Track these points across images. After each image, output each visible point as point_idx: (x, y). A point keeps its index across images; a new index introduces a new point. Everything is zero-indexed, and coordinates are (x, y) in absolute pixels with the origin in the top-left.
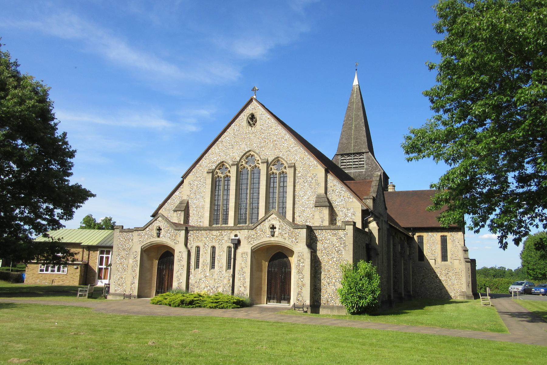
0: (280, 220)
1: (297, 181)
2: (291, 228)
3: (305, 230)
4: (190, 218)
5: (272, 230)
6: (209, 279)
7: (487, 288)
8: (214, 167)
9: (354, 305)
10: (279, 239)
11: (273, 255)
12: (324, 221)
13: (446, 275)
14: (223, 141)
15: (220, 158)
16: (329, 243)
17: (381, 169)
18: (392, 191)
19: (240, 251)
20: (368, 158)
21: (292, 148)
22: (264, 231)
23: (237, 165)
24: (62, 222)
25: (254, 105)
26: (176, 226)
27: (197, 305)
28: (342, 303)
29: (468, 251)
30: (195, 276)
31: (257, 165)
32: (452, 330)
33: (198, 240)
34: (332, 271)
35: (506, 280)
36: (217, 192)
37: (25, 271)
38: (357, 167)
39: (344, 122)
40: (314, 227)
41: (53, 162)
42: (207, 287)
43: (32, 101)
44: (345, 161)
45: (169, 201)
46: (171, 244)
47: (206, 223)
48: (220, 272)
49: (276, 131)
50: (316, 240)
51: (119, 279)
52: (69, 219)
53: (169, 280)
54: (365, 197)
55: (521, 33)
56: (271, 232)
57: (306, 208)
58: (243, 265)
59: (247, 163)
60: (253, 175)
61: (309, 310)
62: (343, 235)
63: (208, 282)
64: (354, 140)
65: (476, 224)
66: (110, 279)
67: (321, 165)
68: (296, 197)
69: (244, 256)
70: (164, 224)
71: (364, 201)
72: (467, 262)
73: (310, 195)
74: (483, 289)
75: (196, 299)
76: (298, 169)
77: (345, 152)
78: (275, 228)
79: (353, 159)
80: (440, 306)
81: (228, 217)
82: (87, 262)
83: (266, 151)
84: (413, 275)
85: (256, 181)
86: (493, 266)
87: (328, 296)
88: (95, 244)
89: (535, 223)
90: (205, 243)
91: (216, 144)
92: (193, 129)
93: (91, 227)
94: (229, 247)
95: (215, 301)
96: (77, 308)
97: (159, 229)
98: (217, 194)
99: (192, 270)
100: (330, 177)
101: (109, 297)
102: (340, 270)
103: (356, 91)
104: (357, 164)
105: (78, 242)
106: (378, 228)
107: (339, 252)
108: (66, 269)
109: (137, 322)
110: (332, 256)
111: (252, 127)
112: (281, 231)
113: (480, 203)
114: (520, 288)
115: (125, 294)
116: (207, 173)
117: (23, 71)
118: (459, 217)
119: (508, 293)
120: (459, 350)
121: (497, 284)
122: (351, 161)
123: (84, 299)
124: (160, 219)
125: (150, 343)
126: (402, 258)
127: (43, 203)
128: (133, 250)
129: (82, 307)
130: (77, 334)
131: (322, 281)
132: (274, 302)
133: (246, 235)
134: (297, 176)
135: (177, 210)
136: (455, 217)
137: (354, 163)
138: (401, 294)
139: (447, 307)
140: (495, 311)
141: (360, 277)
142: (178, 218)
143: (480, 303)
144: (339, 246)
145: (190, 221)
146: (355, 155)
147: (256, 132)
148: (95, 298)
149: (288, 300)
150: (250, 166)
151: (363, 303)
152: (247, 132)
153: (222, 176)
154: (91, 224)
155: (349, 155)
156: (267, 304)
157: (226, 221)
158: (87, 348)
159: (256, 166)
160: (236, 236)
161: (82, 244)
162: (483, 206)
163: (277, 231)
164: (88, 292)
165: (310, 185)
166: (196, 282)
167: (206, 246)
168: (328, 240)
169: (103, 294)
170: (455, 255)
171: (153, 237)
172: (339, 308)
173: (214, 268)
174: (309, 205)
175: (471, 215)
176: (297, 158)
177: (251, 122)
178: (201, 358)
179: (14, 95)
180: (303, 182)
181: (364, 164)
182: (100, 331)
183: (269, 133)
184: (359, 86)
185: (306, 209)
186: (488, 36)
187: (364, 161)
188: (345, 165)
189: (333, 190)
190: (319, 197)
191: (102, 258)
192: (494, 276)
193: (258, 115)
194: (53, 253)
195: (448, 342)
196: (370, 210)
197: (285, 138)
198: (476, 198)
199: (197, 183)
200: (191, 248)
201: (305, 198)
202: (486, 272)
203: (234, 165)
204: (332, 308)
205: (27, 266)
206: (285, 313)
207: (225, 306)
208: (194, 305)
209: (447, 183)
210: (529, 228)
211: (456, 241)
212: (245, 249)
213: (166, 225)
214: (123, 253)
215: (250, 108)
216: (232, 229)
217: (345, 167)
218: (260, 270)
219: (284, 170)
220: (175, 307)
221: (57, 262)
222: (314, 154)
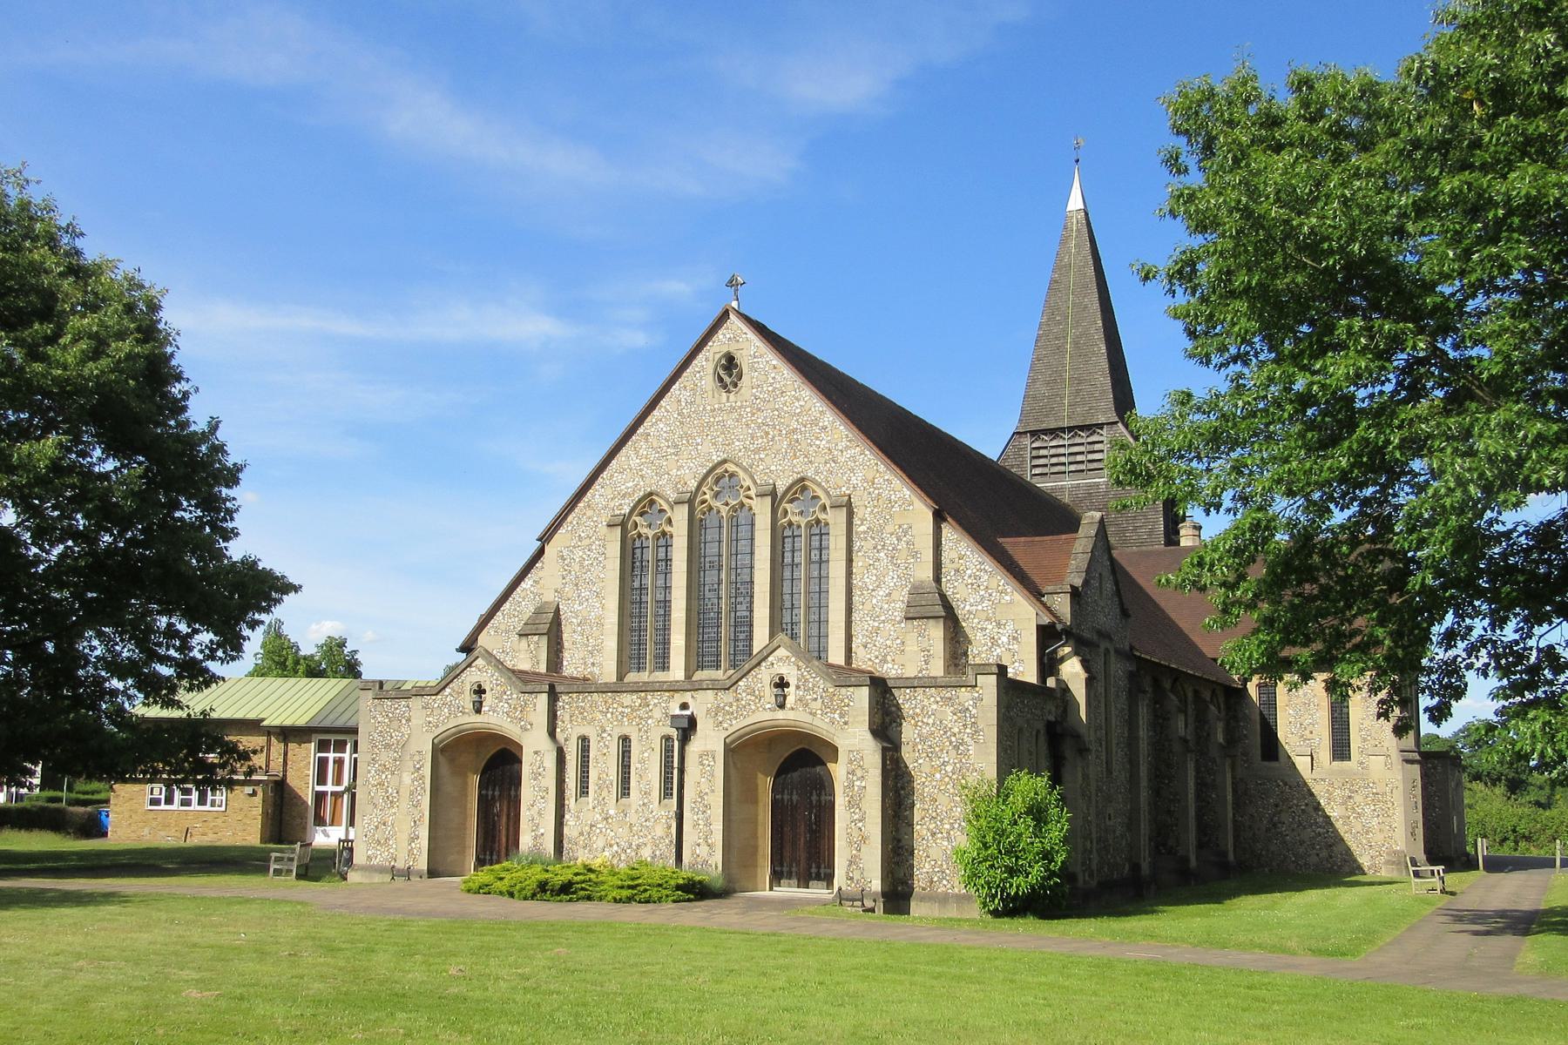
0: (800, 664)
1: (857, 545)
3: (865, 691)
4: (566, 655)
5: (779, 691)
8: (626, 510)
9: (996, 892)
10: (796, 715)
15: (642, 483)
16: (933, 724)
18: (1190, 544)
19: (694, 748)
21: (842, 451)
22: (757, 692)
23: (691, 502)
24: (213, 666)
26: (524, 679)
27: (582, 893)
31: (746, 501)
33: (584, 718)
34: (943, 800)
37: (107, 801)
38: (1083, 471)
39: (1040, 329)
40: (892, 681)
41: (185, 503)
42: (611, 846)
44: (1043, 452)
45: (507, 606)
46: (510, 729)
47: (607, 670)
48: (644, 804)
49: (796, 404)
50: (898, 716)
52: (233, 659)
53: (511, 829)
54: (1050, 588)
57: (883, 622)
58: (705, 788)
59: (716, 495)
60: (734, 529)
61: (880, 906)
63: (613, 834)
66: (352, 823)
68: (856, 592)
70: (492, 676)
73: (892, 584)
76: (859, 513)
77: (1044, 426)
78: (787, 685)
81: (669, 649)
82: (281, 775)
83: (768, 460)
85: (743, 546)
88: (302, 721)
91: (630, 443)
94: (668, 738)
95: (631, 883)
96: (277, 902)
97: (480, 691)
99: (570, 801)
101: (353, 877)
103: (1078, 230)
104: (1082, 462)
105: (251, 716)
106: (1086, 675)
109: (427, 932)
111: (729, 392)
112: (801, 693)
115: (393, 867)
116: (609, 526)
117: (92, 251)
121: (1554, 827)
122: (1061, 451)
123: (286, 881)
124: (480, 662)
125: (452, 971)
127: (160, 613)
128: (413, 748)
129: (291, 902)
130: (295, 955)
131: (917, 828)
132: (790, 886)
133: (709, 706)
134: (857, 532)
137: (1072, 459)
141: (1013, 815)
142: (530, 656)
144: (959, 733)
145: (565, 663)
146: (1076, 433)
147: (740, 408)
148: (317, 879)
149: (829, 879)
150: (727, 504)
152: (716, 406)
153: (650, 533)
154: (286, 660)
155: (1054, 432)
156: (771, 889)
157: (663, 663)
158: (323, 978)
159: (742, 505)
160: (684, 706)
161: (265, 723)
164: (295, 863)
165: (893, 558)
166: (581, 834)
167: (604, 735)
168: (929, 717)
170: (1373, 742)
171: (463, 713)
172: (961, 899)
173: (629, 794)
174: (890, 613)
176: (855, 482)
177: (727, 379)
178: (555, 996)
179: (80, 332)
180: (875, 548)
182: (343, 950)
184: (1086, 214)
185: (882, 625)
187: (1102, 451)
188: (1046, 465)
189: (957, 571)
190: (916, 591)
191: (322, 763)
193: (746, 358)
194: (193, 751)
196: (1059, 627)
197: (821, 424)
199: (581, 553)
200: (566, 740)
201: (881, 593)
204: (944, 899)
205: (113, 791)
207: (655, 895)
208: (574, 893)
212: (709, 743)
213: (497, 680)
214: (385, 757)
215: (721, 337)
216: (673, 688)
217: (1045, 470)
218: (751, 797)
219: (822, 516)
220: (525, 899)
221: (208, 780)
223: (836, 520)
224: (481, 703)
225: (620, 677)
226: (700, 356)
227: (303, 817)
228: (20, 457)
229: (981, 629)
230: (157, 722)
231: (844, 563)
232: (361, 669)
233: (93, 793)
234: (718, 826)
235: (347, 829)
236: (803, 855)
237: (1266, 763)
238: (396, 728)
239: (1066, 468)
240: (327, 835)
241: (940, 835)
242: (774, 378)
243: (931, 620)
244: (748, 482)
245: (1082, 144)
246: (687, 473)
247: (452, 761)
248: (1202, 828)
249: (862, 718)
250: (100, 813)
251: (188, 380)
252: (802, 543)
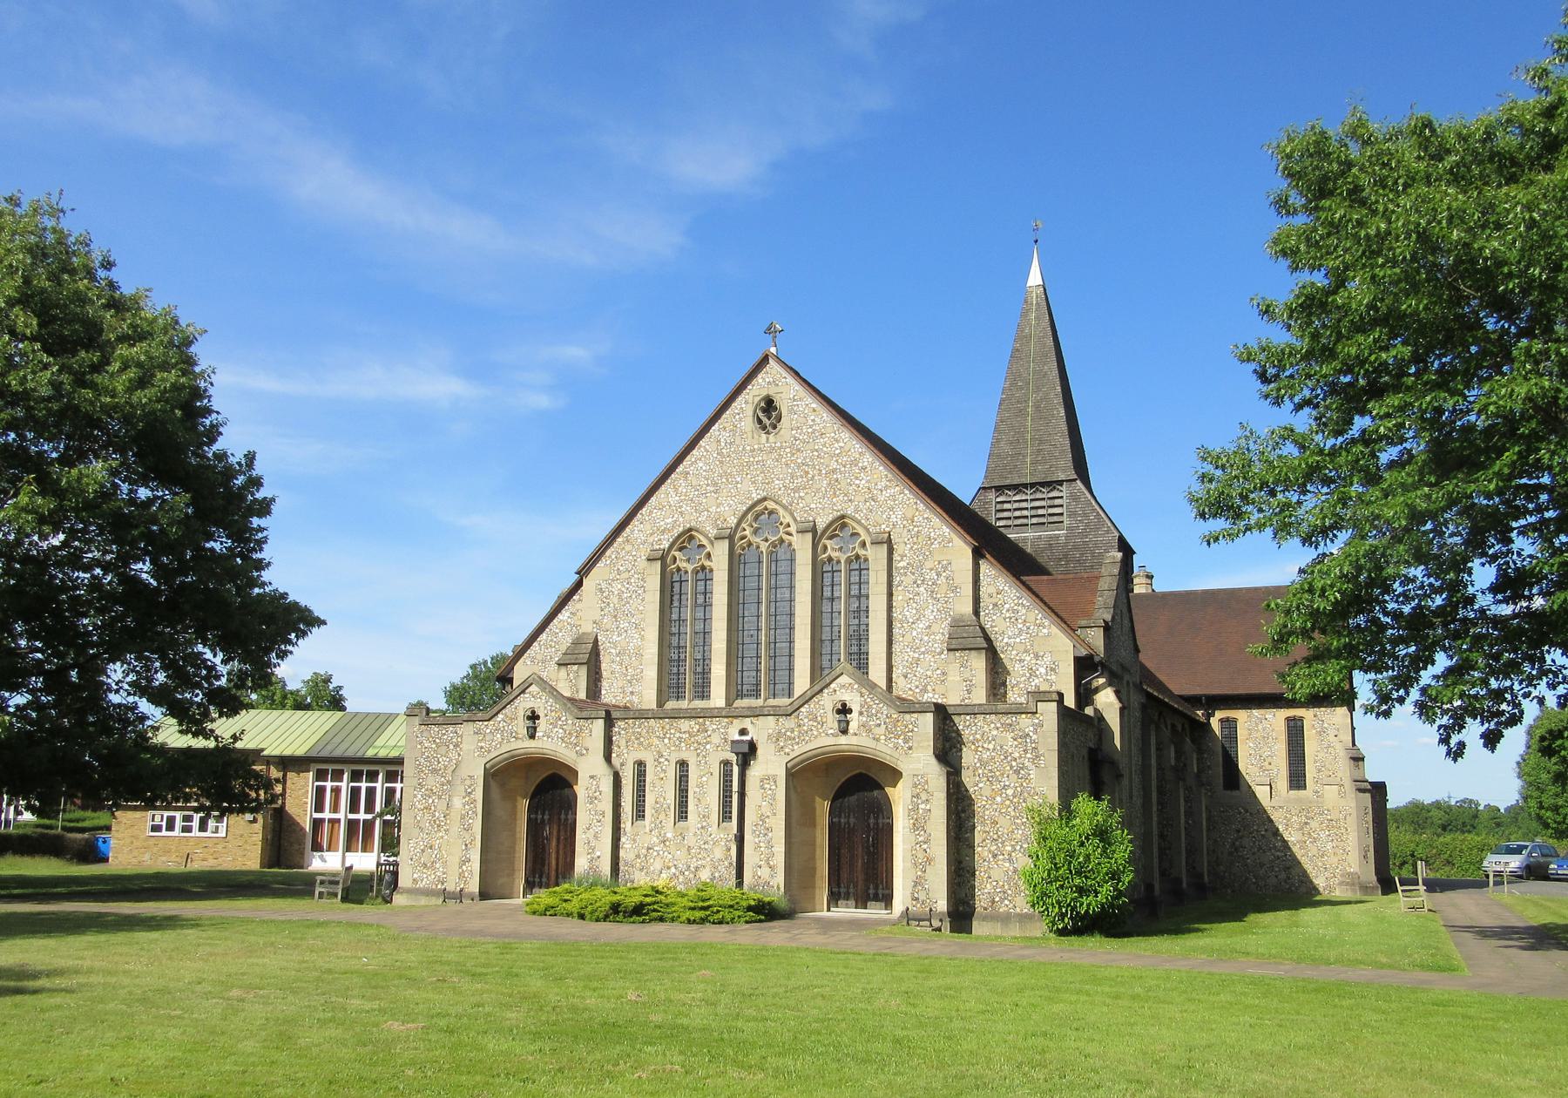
0: (863, 690)
2: (893, 711)
3: (930, 717)
4: (605, 684)
5: (842, 717)
6: (673, 850)
7: (1419, 862)
8: (666, 545)
9: (1067, 911)
10: (860, 740)
11: (843, 783)
12: (973, 689)
13: (1301, 829)
14: (688, 473)
15: (681, 519)
17: (1112, 528)
19: (755, 771)
20: (1074, 497)
22: (819, 718)
23: (731, 538)
25: (774, 372)
27: (655, 914)
28: (1033, 906)
29: (1363, 759)
30: (634, 840)
31: (785, 537)
32: (1323, 967)
33: (641, 744)
34: (1004, 822)
35: (1473, 838)
36: (675, 610)
37: (108, 828)
40: (952, 708)
42: (669, 868)
43: (170, 372)
44: (1006, 506)
45: (543, 636)
46: (565, 754)
47: (647, 697)
48: (702, 827)
49: (836, 445)
51: (423, 851)
54: (1083, 623)
55: (1487, 251)
56: (839, 721)
57: (923, 653)
58: (766, 810)
59: (756, 532)
61: (947, 925)
62: (1031, 729)
64: (1032, 446)
65: (1384, 698)
67: (959, 537)
68: (896, 625)
69: (768, 786)
71: (1079, 632)
72: (1361, 790)
73: (932, 617)
74: (1408, 867)
75: (648, 900)
76: (899, 549)
77: (1008, 482)
78: (850, 711)
79: (1032, 500)
80: (1288, 912)
83: (808, 499)
84: (1208, 830)
85: (783, 579)
86: (1439, 798)
87: (995, 888)
88: (301, 752)
89: (1535, 693)
90: (659, 752)
92: (543, 401)
93: (274, 701)
94: (726, 764)
95: (701, 904)
97: (533, 717)
98: (675, 616)
99: (626, 824)
100: (988, 569)
101: (399, 899)
102: (1025, 820)
106: (1120, 705)
107: (1022, 772)
108: (223, 826)
110: (1002, 784)
111: (768, 433)
112: (864, 719)
113: (1396, 641)
114: (1515, 862)
118: (1342, 680)
119: (1479, 876)
120: (1342, 1007)
122: (1024, 505)
123: (332, 903)
126: (1181, 783)
128: (464, 772)
131: (978, 849)
133: (770, 731)
134: (896, 568)
136: (1329, 679)
137: (1034, 512)
138: (1178, 881)
139: (1307, 915)
140: (1437, 924)
141: (1080, 837)
142: (573, 683)
143: (1397, 905)
144: (1020, 757)
145: (603, 692)
147: (780, 448)
149: (887, 900)
150: (766, 540)
151: (1089, 905)
152: (756, 447)
153: (690, 568)
154: (274, 694)
155: (1017, 488)
156: (829, 910)
157: (703, 691)
159: (782, 541)
160: (743, 732)
161: (265, 753)
162: (1402, 651)
163: (854, 720)
164: (341, 886)
166: (638, 856)
167: (662, 760)
168: (990, 742)
169: (372, 891)
171: (517, 738)
172: (1023, 918)
173: (686, 817)
175: (1372, 676)
177: (765, 420)
180: (915, 583)
181: (1062, 514)
183: (817, 451)
184: (1045, 290)
186: (1408, 257)
187: (1062, 506)
189: (995, 605)
190: (957, 624)
191: (320, 792)
192: (1444, 828)
195: (1316, 991)
196: (1097, 659)
197: (860, 465)
198: (1383, 628)
199: (619, 586)
200: (622, 765)
201: (921, 626)
202: (1418, 815)
203: (723, 538)
204: (1006, 919)
205: (115, 818)
206: (889, 933)
208: (646, 914)
209: (1307, 600)
210: (1520, 704)
211: (1332, 733)
212: (770, 768)
213: (551, 706)
214: (432, 781)
215: (760, 381)
216: (729, 713)
217: (1009, 523)
218: (810, 820)
219: (862, 552)
222: (941, 508)
223: (876, 556)
224: (535, 728)
225: (660, 704)
226: (740, 398)
227: (301, 843)
228: (68, 482)
229: (1020, 661)
230: (188, 752)
231: (885, 597)
232: (346, 704)
233: (78, 821)
234: (780, 849)
235: (344, 855)
236: (860, 876)
237: (1229, 792)
239: (1029, 521)
240: (324, 860)
241: (1001, 857)
243: (973, 652)
244: (788, 519)
245: (1040, 226)
246: (728, 510)
247: (502, 785)
248: (1189, 852)
249: (927, 743)
250: (97, 839)
251: (218, 413)
252: (842, 577)
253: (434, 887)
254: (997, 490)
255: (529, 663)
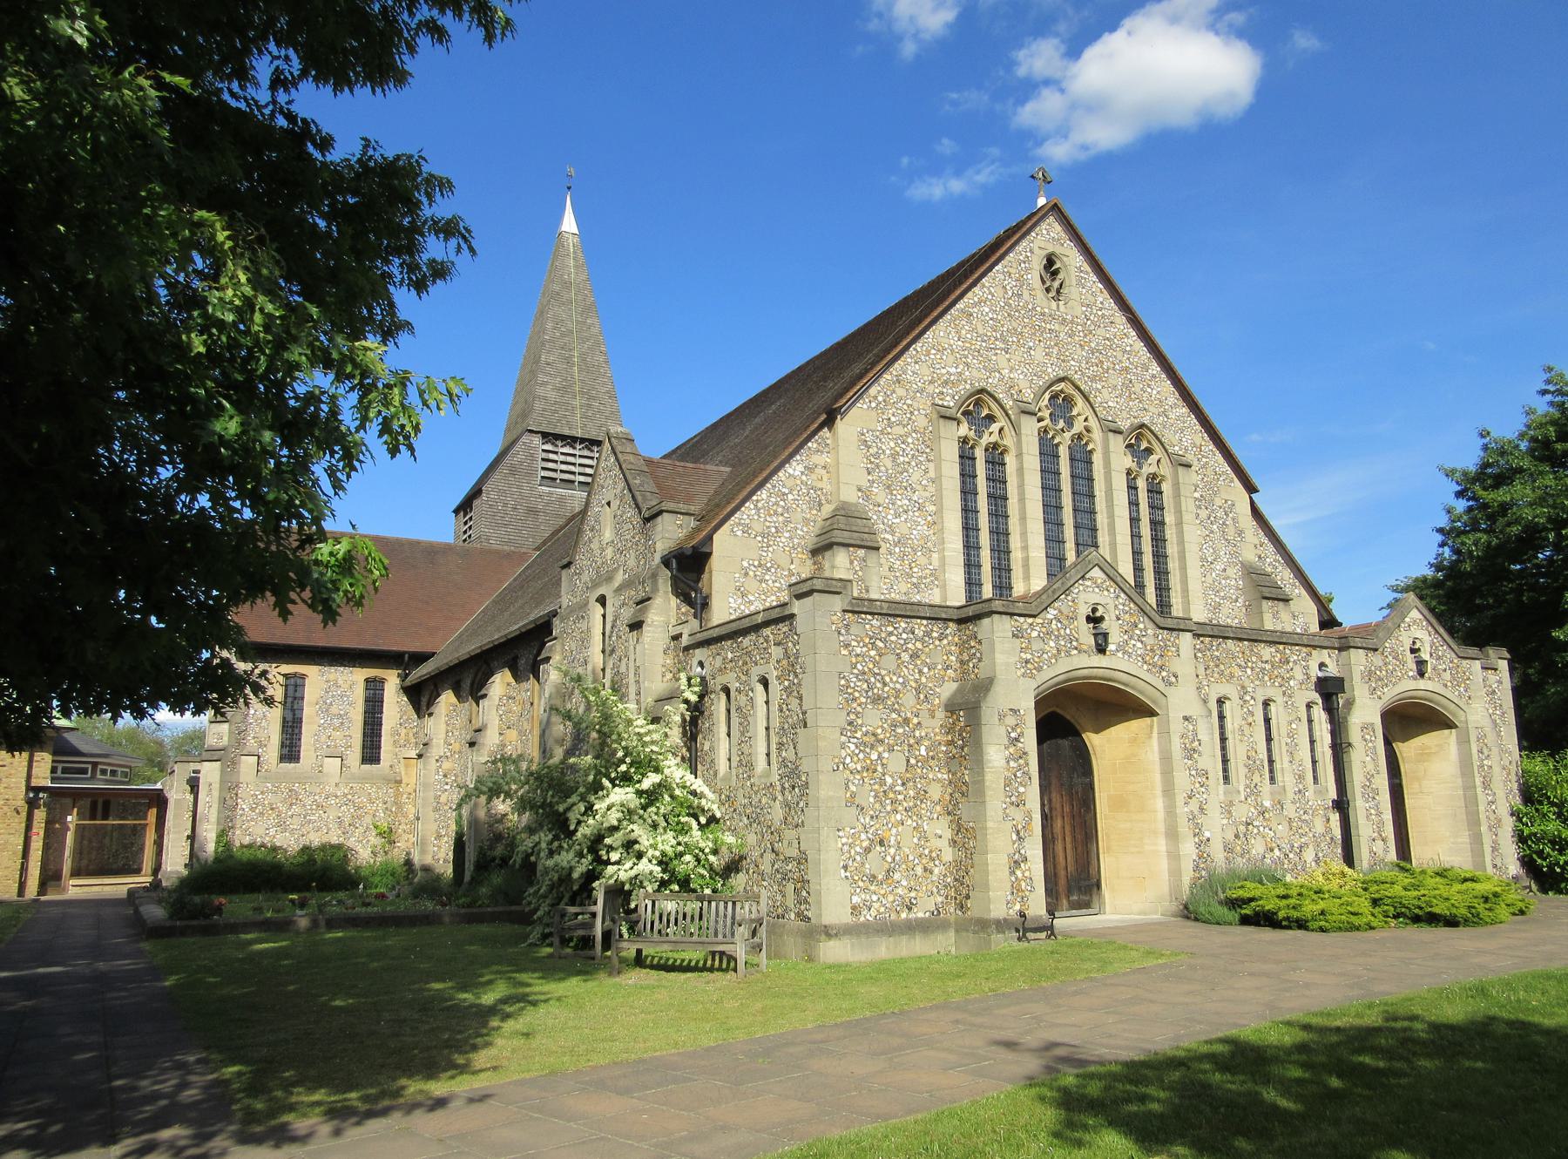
15: (967, 373)
33: (1221, 673)
44: (552, 456)
48: (1300, 791)
51: (868, 850)
57: (1223, 598)
90: (1243, 687)
91: (949, 317)
103: (575, 252)
135: (852, 542)
137: (582, 470)
147: (1072, 322)
152: (1046, 310)
166: (1237, 836)
238: (893, 667)
242: (1102, 303)
253: (893, 916)
254: (544, 437)
255: (739, 533)
